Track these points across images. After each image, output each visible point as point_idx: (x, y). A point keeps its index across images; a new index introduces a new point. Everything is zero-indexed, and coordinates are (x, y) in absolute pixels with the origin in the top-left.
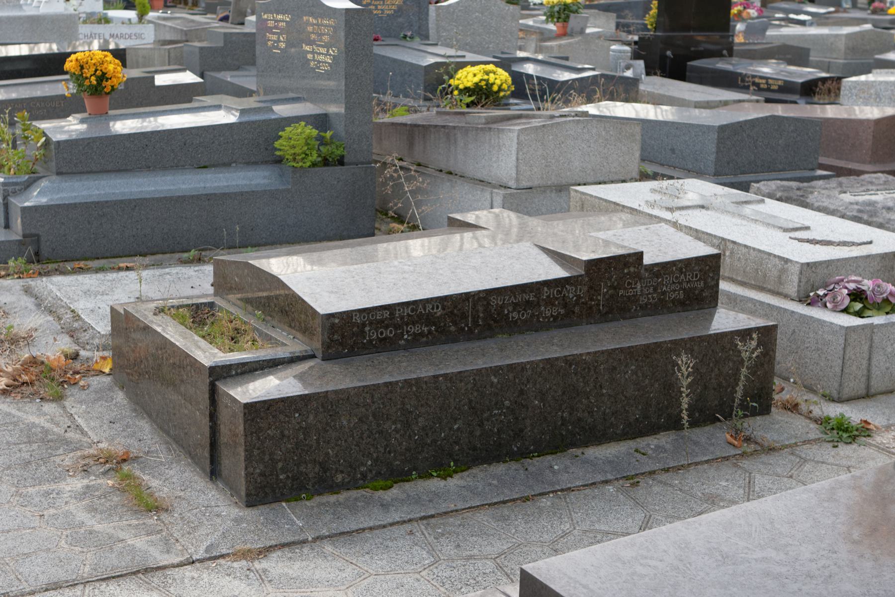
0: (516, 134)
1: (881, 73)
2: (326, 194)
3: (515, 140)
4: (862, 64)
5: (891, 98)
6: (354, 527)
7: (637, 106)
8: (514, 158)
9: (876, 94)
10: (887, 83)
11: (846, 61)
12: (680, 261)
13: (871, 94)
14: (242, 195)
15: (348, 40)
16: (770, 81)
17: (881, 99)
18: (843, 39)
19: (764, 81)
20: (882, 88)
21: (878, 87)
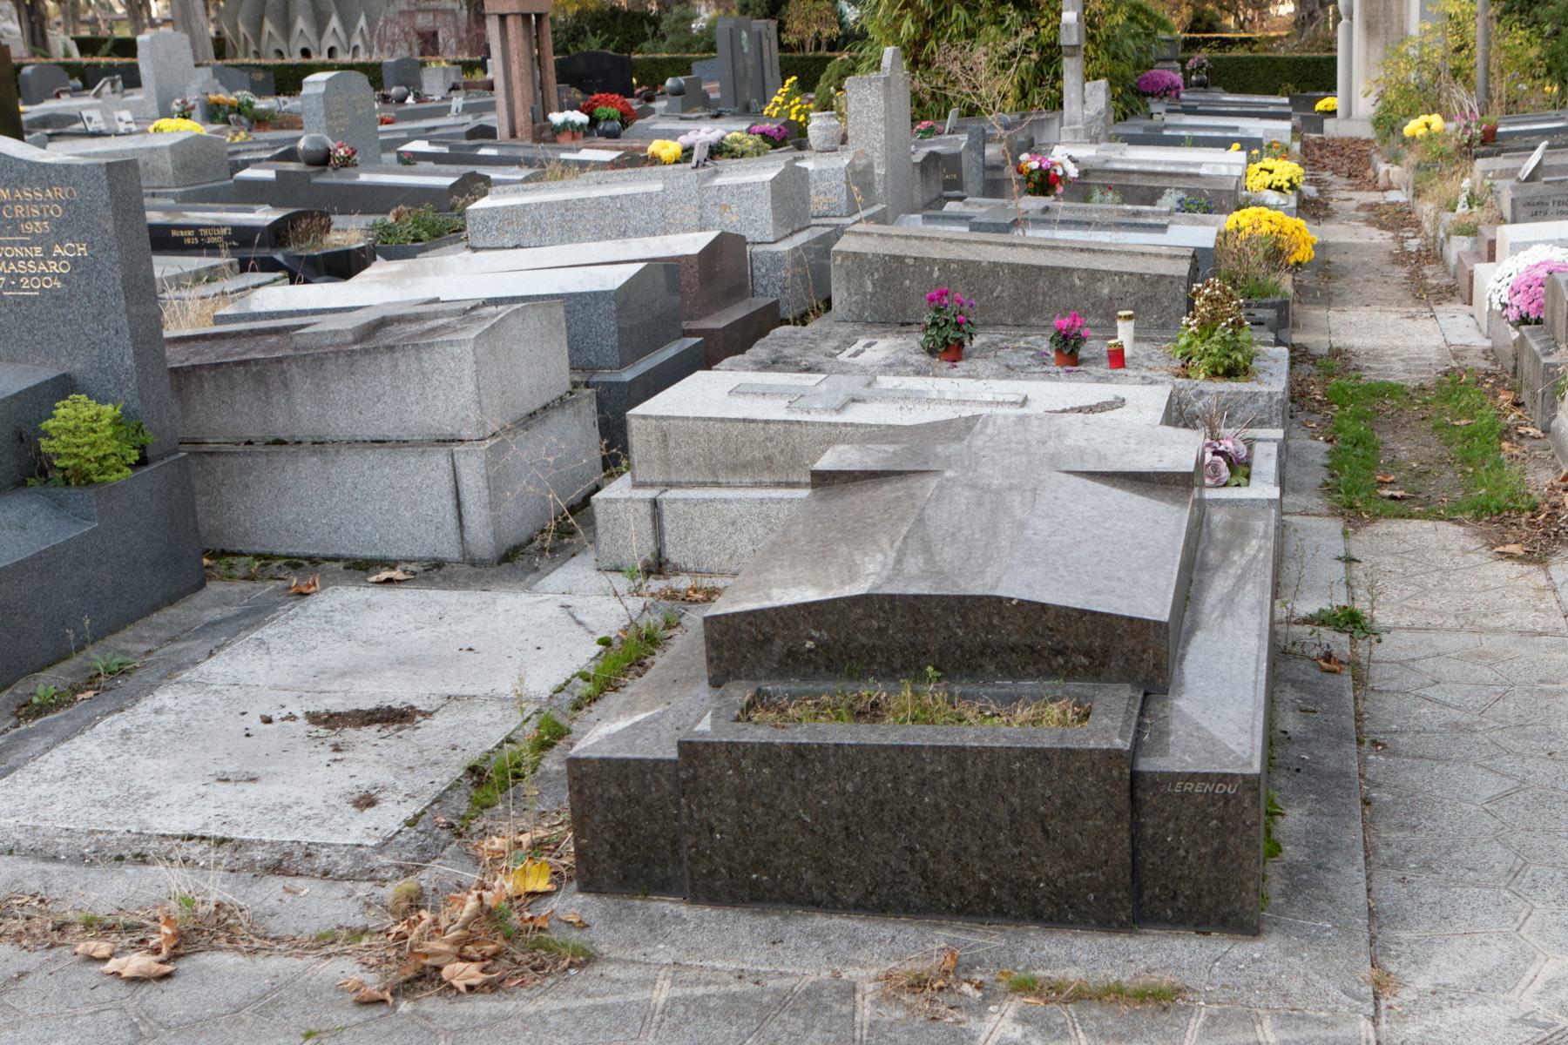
0: (469, 347)
1: (505, 192)
2: (141, 523)
3: (470, 358)
4: (202, 190)
5: (563, 227)
6: (1531, 977)
7: (1010, 260)
8: (472, 388)
9: (533, 223)
10: (549, 204)
11: (183, 190)
12: (1179, 473)
13: (525, 225)
14: (41, 558)
15: (119, 223)
16: (204, 232)
17: (544, 231)
18: (168, 155)
19: (190, 233)
20: (543, 212)
21: (536, 213)
